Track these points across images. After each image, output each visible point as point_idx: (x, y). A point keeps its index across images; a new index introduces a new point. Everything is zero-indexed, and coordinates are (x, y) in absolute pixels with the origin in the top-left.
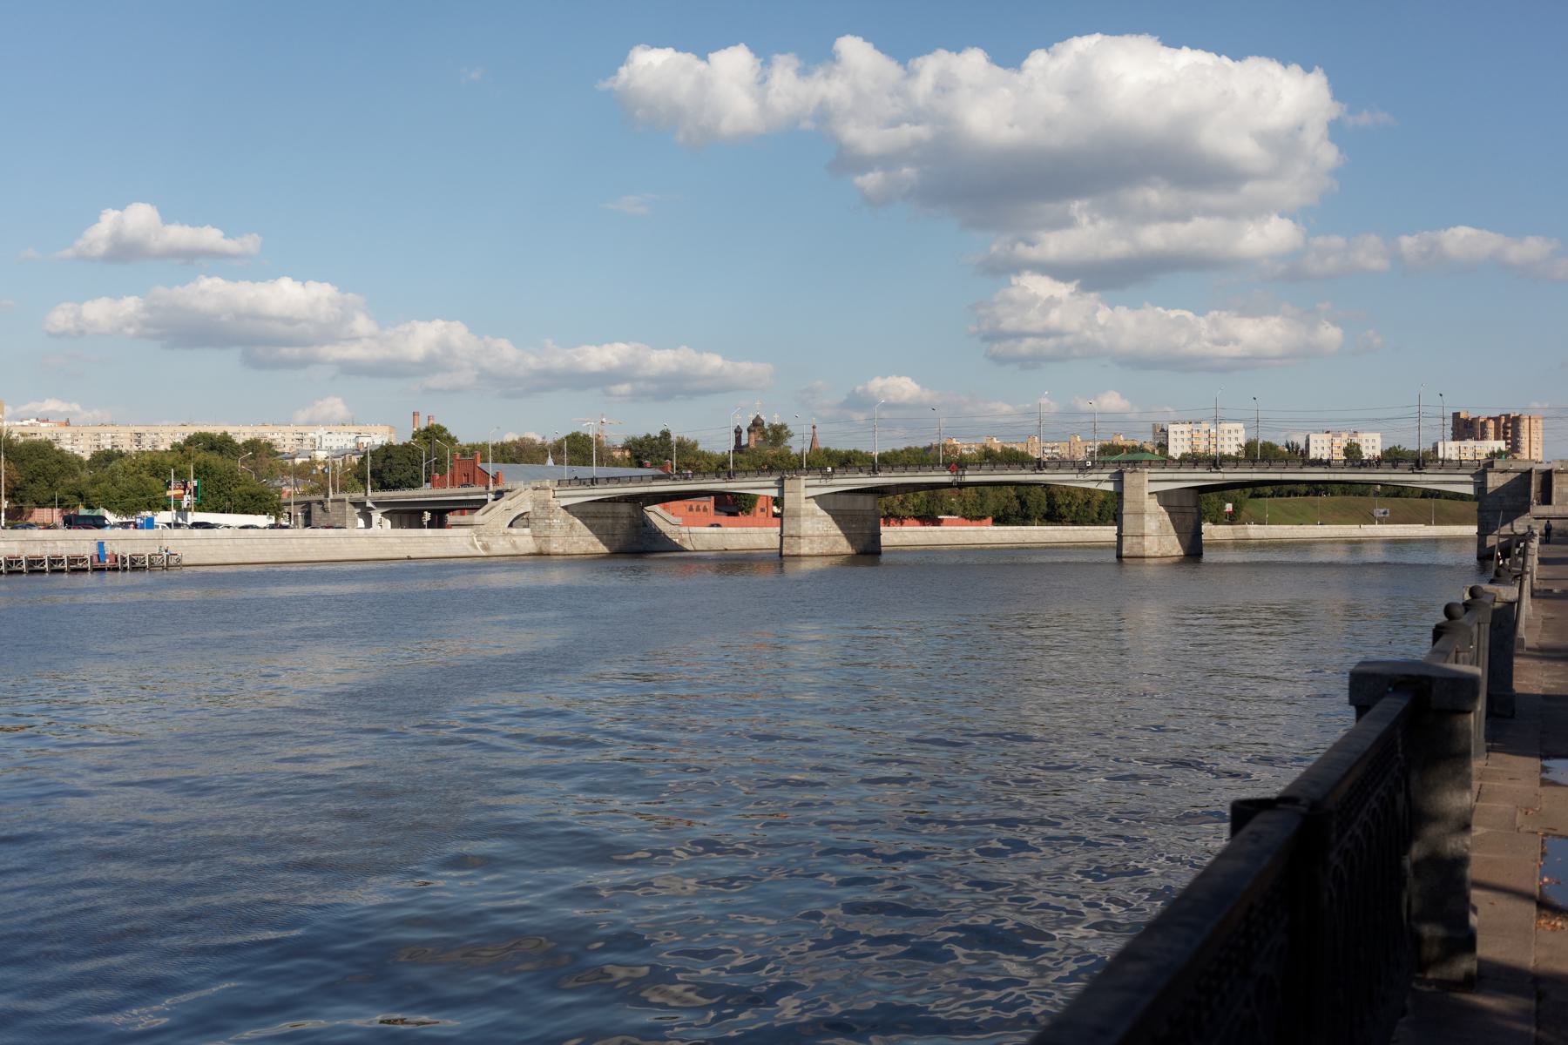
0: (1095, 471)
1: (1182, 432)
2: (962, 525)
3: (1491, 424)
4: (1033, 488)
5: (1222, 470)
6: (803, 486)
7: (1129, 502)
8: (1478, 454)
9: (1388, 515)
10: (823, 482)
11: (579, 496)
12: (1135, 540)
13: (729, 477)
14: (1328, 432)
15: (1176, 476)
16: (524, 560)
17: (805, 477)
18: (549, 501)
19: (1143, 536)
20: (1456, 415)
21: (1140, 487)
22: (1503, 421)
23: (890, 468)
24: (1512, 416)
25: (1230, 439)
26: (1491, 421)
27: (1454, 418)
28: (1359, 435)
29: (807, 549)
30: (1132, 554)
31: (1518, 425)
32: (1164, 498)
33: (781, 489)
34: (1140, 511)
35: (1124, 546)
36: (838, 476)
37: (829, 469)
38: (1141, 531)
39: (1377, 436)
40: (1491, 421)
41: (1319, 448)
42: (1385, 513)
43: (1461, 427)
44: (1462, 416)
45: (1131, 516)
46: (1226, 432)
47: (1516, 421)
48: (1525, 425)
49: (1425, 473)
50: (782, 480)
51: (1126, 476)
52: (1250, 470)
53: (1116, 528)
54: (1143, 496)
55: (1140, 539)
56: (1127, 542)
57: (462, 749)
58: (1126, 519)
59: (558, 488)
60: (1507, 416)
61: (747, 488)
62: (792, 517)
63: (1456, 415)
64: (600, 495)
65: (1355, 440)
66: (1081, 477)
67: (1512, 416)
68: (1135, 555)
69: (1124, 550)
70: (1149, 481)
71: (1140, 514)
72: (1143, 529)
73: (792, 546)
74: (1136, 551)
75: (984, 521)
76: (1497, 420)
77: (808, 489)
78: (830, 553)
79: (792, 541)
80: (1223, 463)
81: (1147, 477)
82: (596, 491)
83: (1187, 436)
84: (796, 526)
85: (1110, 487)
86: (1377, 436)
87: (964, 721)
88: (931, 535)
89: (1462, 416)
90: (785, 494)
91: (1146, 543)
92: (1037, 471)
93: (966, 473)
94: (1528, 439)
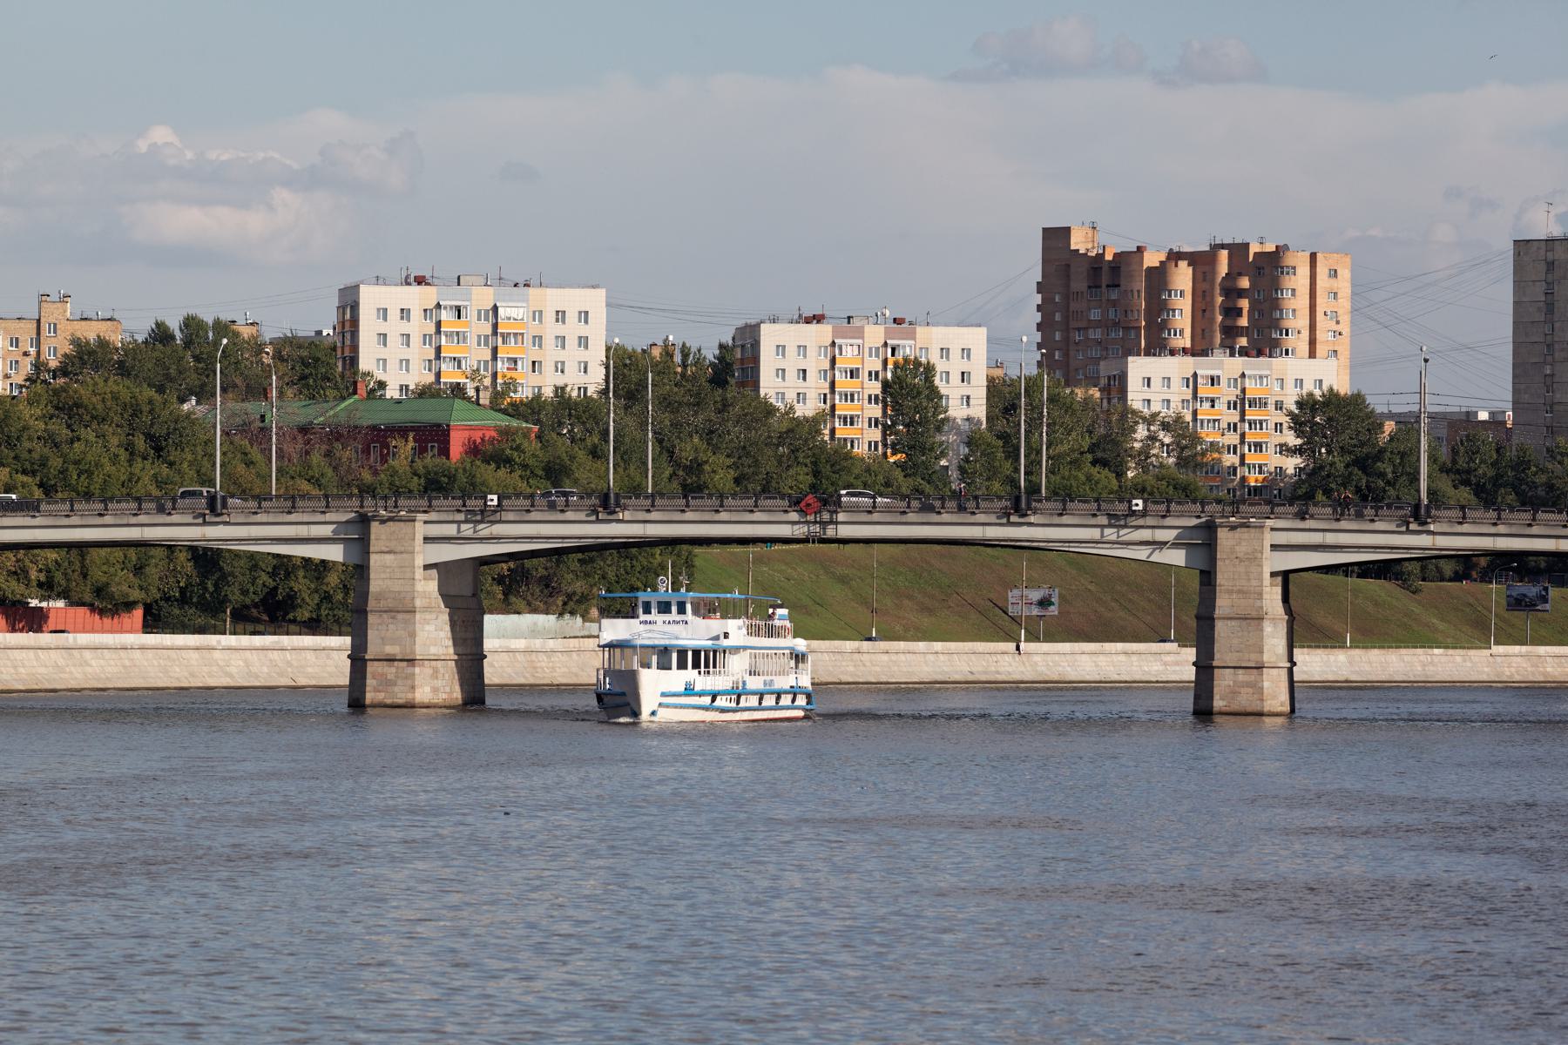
0: (1149, 521)
1: (405, 313)
2: (93, 631)
3: (1183, 277)
5: (1432, 527)
7: (1230, 592)
8: (1252, 403)
9: (1053, 610)
10: (467, 529)
12: (1242, 676)
14: (818, 319)
15: (1330, 538)
16: (15, 700)
19: (1260, 668)
20: (1055, 238)
21: (1254, 559)
22: (1223, 268)
24: (1254, 248)
25: (561, 341)
26: (1183, 264)
27: (1046, 249)
28: (921, 331)
29: (427, 689)
30: (1235, 707)
31: (1276, 286)
33: (362, 544)
34: (1254, 614)
35: (1216, 690)
36: (511, 516)
37: (493, 499)
38: (1253, 656)
39: (595, 301)
40: (1183, 264)
41: (792, 375)
42: (1044, 603)
43: (1079, 284)
44: (1078, 242)
45: (1233, 623)
46: (549, 317)
47: (1270, 267)
48: (1297, 282)
50: (364, 521)
51: (1222, 534)
52: (1493, 530)
53: (348, 640)
54: (1261, 580)
55: (1251, 676)
56: (1223, 681)
58: (1220, 626)
60: (1238, 251)
61: (257, 540)
62: (392, 611)
63: (1055, 238)
65: (908, 349)
66: (1110, 534)
67: (1254, 248)
68: (1243, 710)
69: (1216, 697)
70: (425, 539)
71: (404, 610)
72: (1262, 652)
73: (392, 683)
74: (1245, 701)
75: (126, 619)
76: (1201, 262)
77: (431, 547)
78: (963, 680)
79: (390, 671)
80: (1433, 512)
81: (1270, 538)
83: (419, 326)
84: (401, 633)
86: (595, 301)
87: (1374, 966)
89: (1078, 242)
90: (375, 560)
91: (1266, 684)
92: (1014, 519)
93: (841, 517)
94: (1305, 334)
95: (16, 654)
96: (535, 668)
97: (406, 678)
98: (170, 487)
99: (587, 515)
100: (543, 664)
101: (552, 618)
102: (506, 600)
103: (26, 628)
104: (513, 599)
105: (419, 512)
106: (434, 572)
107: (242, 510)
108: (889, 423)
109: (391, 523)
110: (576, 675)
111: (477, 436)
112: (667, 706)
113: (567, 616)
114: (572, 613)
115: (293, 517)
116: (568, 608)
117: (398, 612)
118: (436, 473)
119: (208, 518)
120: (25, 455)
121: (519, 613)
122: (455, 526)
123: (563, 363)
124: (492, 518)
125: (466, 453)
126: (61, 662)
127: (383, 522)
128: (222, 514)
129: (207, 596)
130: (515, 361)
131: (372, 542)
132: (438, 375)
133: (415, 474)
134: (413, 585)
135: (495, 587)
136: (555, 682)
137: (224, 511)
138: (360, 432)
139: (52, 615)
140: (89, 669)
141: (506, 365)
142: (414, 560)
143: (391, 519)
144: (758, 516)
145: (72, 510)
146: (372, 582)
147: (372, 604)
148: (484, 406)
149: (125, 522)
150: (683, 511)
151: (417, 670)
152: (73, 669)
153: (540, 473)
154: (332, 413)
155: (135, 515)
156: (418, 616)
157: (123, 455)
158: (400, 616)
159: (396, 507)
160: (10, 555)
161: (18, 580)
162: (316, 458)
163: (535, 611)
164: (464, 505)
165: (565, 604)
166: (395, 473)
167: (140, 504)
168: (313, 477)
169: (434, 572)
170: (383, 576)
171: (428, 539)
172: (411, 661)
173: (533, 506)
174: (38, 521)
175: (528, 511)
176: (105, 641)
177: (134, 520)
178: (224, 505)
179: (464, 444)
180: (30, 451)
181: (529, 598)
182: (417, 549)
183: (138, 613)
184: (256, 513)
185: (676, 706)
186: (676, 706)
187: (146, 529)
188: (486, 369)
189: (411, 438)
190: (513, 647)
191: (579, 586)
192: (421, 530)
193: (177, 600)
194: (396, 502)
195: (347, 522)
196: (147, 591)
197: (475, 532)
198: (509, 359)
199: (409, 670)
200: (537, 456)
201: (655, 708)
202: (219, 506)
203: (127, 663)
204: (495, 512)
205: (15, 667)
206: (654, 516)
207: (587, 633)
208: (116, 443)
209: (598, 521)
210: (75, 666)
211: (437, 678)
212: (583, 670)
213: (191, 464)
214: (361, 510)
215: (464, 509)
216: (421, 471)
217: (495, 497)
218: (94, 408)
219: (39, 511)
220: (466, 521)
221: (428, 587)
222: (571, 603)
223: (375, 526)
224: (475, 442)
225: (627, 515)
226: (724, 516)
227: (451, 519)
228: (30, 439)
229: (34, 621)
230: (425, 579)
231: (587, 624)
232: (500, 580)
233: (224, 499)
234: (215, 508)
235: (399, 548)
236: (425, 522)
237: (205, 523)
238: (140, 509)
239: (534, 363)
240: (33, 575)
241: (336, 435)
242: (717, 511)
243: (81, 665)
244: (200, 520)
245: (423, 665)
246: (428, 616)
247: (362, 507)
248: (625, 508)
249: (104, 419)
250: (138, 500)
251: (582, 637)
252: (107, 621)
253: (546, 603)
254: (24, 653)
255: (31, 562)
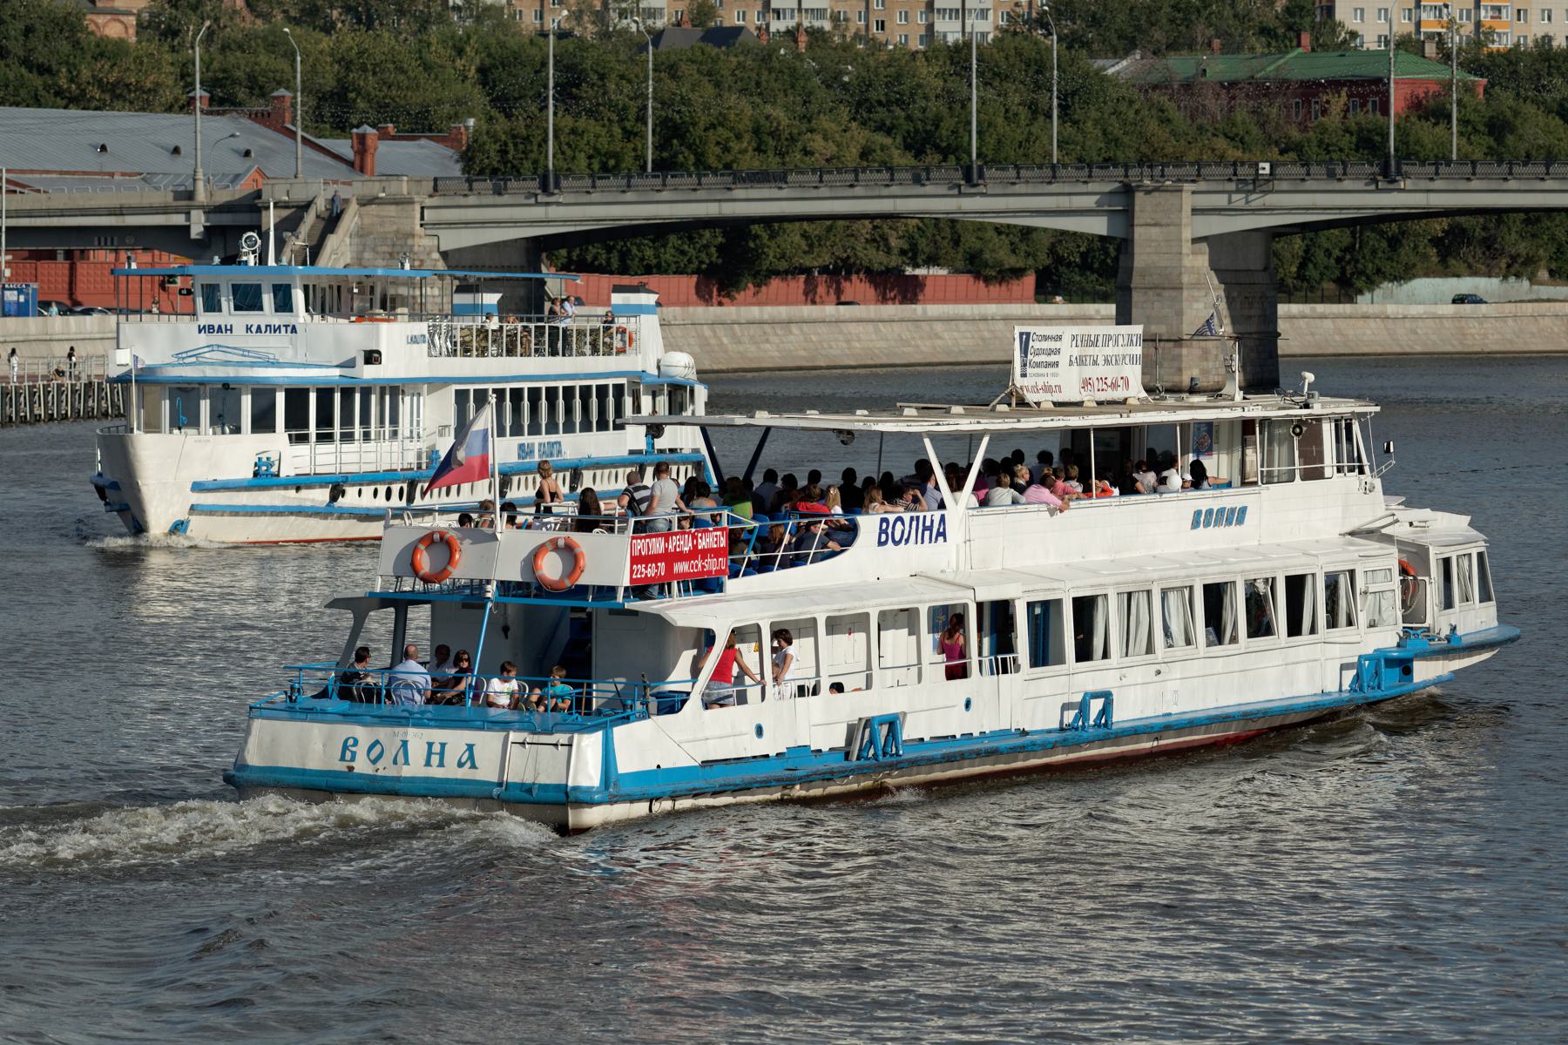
4: (857, 225)
6: (1187, 209)
10: (1239, 200)
11: (515, 223)
13: (545, 188)
17: (1193, 187)
18: (413, 235)
23: (1012, 173)
32: (1216, 244)
33: (1126, 215)
36: (1284, 185)
37: (1265, 168)
49: (558, 204)
50: (1128, 191)
57: (208, 1038)
59: (435, 201)
64: (565, 221)
70: (1193, 210)
77: (1199, 219)
82: (554, 212)
85: (1098, 226)
88: (1474, 328)
90: (1139, 232)
95: (852, 328)
96: (1464, 335)
97: (1173, 359)
98: (1072, 147)
99: (1366, 184)
100: (1473, 331)
101: (1495, 281)
102: (1443, 260)
103: (899, 297)
104: (1452, 261)
105: (1187, 181)
106: (1204, 247)
107: (1001, 181)
108: (675, 141)
109: (1157, 194)
110: (1511, 342)
111: (1421, 92)
112: (211, 511)
113: (1512, 279)
114: (1518, 276)
115: (1054, 188)
116: (1513, 270)
117: (1164, 289)
118: (1369, 131)
119: (963, 189)
120: (917, 114)
121: (1458, 276)
122: (1225, 197)
123: (1550, 11)
124: (1264, 188)
125: (1409, 108)
126: (906, 335)
127: (1148, 192)
128: (977, 185)
129: (1109, 261)
130: (1499, 9)
131: (1137, 214)
132: (1418, 24)
133: (1347, 131)
134: (1180, 260)
135: (1428, 249)
136: (1486, 350)
137: (981, 182)
138: (1288, 88)
139: (928, 283)
140: (939, 342)
141: (1490, 14)
142: (1180, 233)
143: (1156, 190)
144: (1549, 184)
145: (821, 181)
146: (1137, 258)
147: (1136, 281)
148: (1430, 59)
149: (876, 193)
150: (1469, 179)
151: (1184, 351)
152: (919, 342)
153: (1482, 128)
154: (1272, 68)
155: (887, 186)
156: (1185, 293)
157: (1024, 113)
158: (1166, 293)
159: (1163, 176)
160: (867, 222)
161: (878, 249)
162: (1241, 115)
163: (1475, 274)
164: (1235, 174)
165: (1509, 266)
166: (1324, 130)
167: (892, 175)
168: (1237, 135)
169: (1204, 247)
170: (1148, 250)
171: (1196, 211)
172: (1178, 341)
173: (1308, 174)
174: (785, 193)
175: (1303, 180)
176: (961, 312)
177: (885, 191)
178: (981, 176)
179: (1405, 99)
180: (924, 110)
181: (1471, 260)
182: (1184, 221)
183: (1030, 281)
184: (1014, 184)
185: (235, 512)
186: (235, 512)
187: (899, 201)
188: (1468, 18)
189: (1343, 94)
190: (1440, 312)
191: (1523, 248)
192: (1188, 200)
193: (1077, 266)
194: (1162, 171)
195: (1110, 193)
196: (1035, 256)
197: (1247, 202)
198: (1493, 8)
199: (1176, 351)
200: (1479, 111)
201: (183, 516)
202: (975, 176)
203: (986, 334)
204: (1268, 181)
205: (848, 341)
206: (1438, 184)
207: (1534, 297)
208: (1017, 100)
209: (1378, 190)
210: (922, 338)
211: (1207, 360)
212: (1518, 337)
213: (1096, 122)
214: (1126, 180)
215: (1234, 178)
216: (1354, 127)
217: (1267, 166)
218: (997, 66)
219: (786, 182)
220: (1238, 191)
221: (1198, 262)
222: (1516, 265)
223: (1139, 197)
224: (1417, 98)
225: (1409, 184)
226: (1512, 184)
227: (1221, 188)
228: (926, 98)
229: (909, 291)
230: (1193, 253)
231: (1535, 287)
232: (1435, 242)
233: (980, 169)
234: (970, 178)
235: (1165, 221)
236: (1194, 192)
237: (960, 194)
238: (892, 180)
239: (1519, 11)
240: (894, 242)
241: (1261, 90)
242: (1505, 179)
243: (930, 338)
244: (956, 191)
245: (1191, 346)
246: (1196, 293)
247: (1126, 176)
248: (1406, 176)
249: (1007, 77)
250: (891, 169)
251: (1530, 301)
252: (994, 289)
253: (1488, 266)
254: (860, 328)
255: (891, 228)
